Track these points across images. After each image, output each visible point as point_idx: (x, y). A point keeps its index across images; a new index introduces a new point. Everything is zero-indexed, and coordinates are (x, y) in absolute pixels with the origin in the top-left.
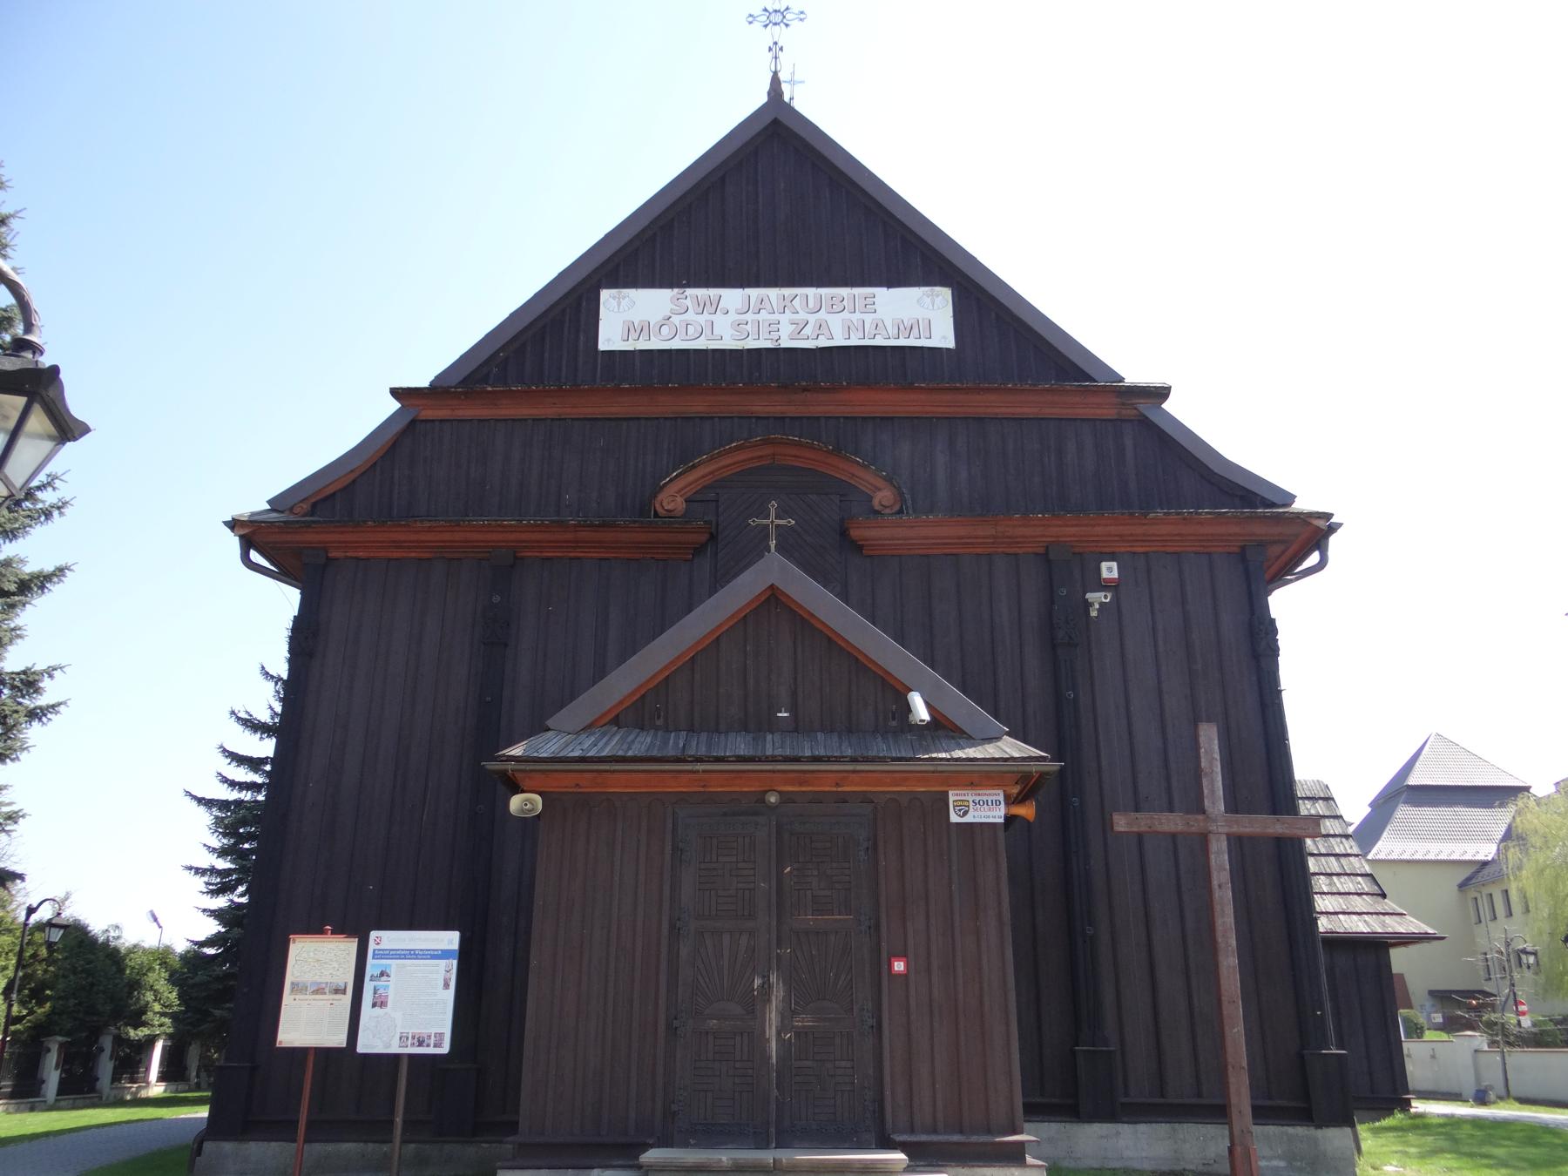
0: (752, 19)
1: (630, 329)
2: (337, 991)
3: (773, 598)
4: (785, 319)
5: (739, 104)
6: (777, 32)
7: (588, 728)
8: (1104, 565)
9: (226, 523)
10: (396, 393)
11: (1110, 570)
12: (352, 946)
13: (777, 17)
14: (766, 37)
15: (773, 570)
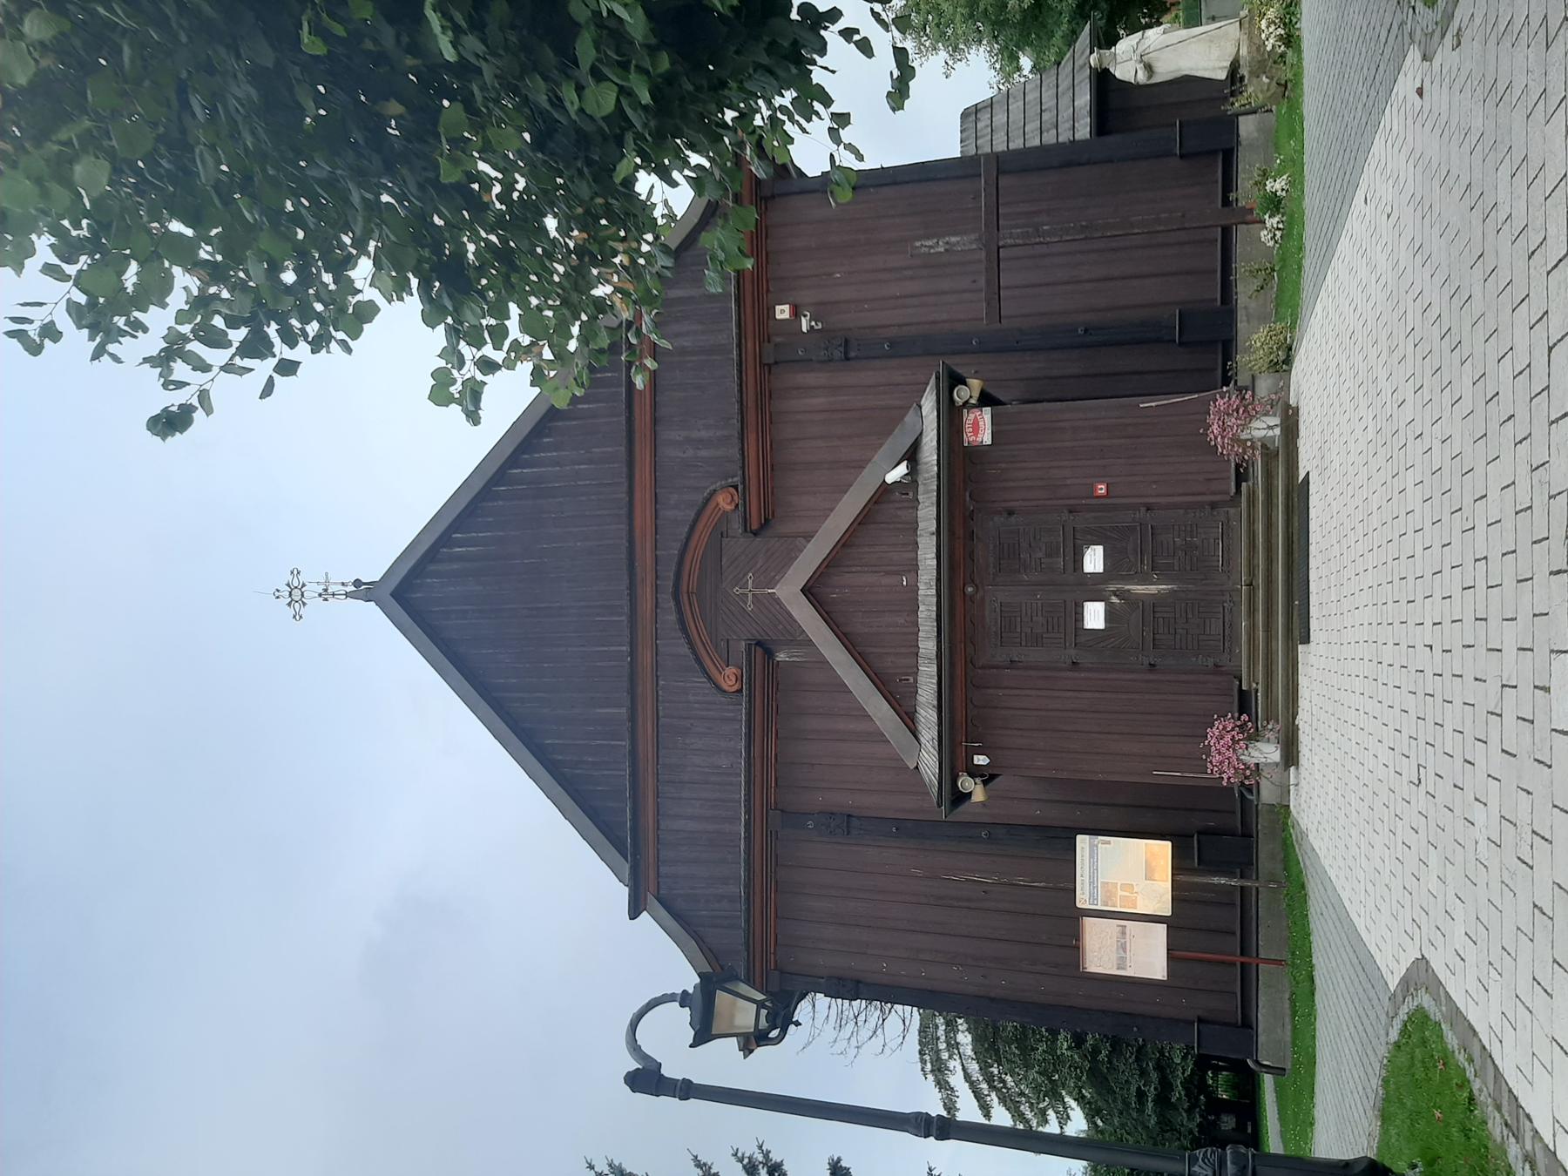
0: (297, 616)
2: (1124, 933)
5: (377, 630)
6: (312, 590)
7: (915, 734)
8: (779, 316)
10: (634, 914)
11: (782, 311)
12: (1088, 922)
13: (295, 595)
14: (314, 604)
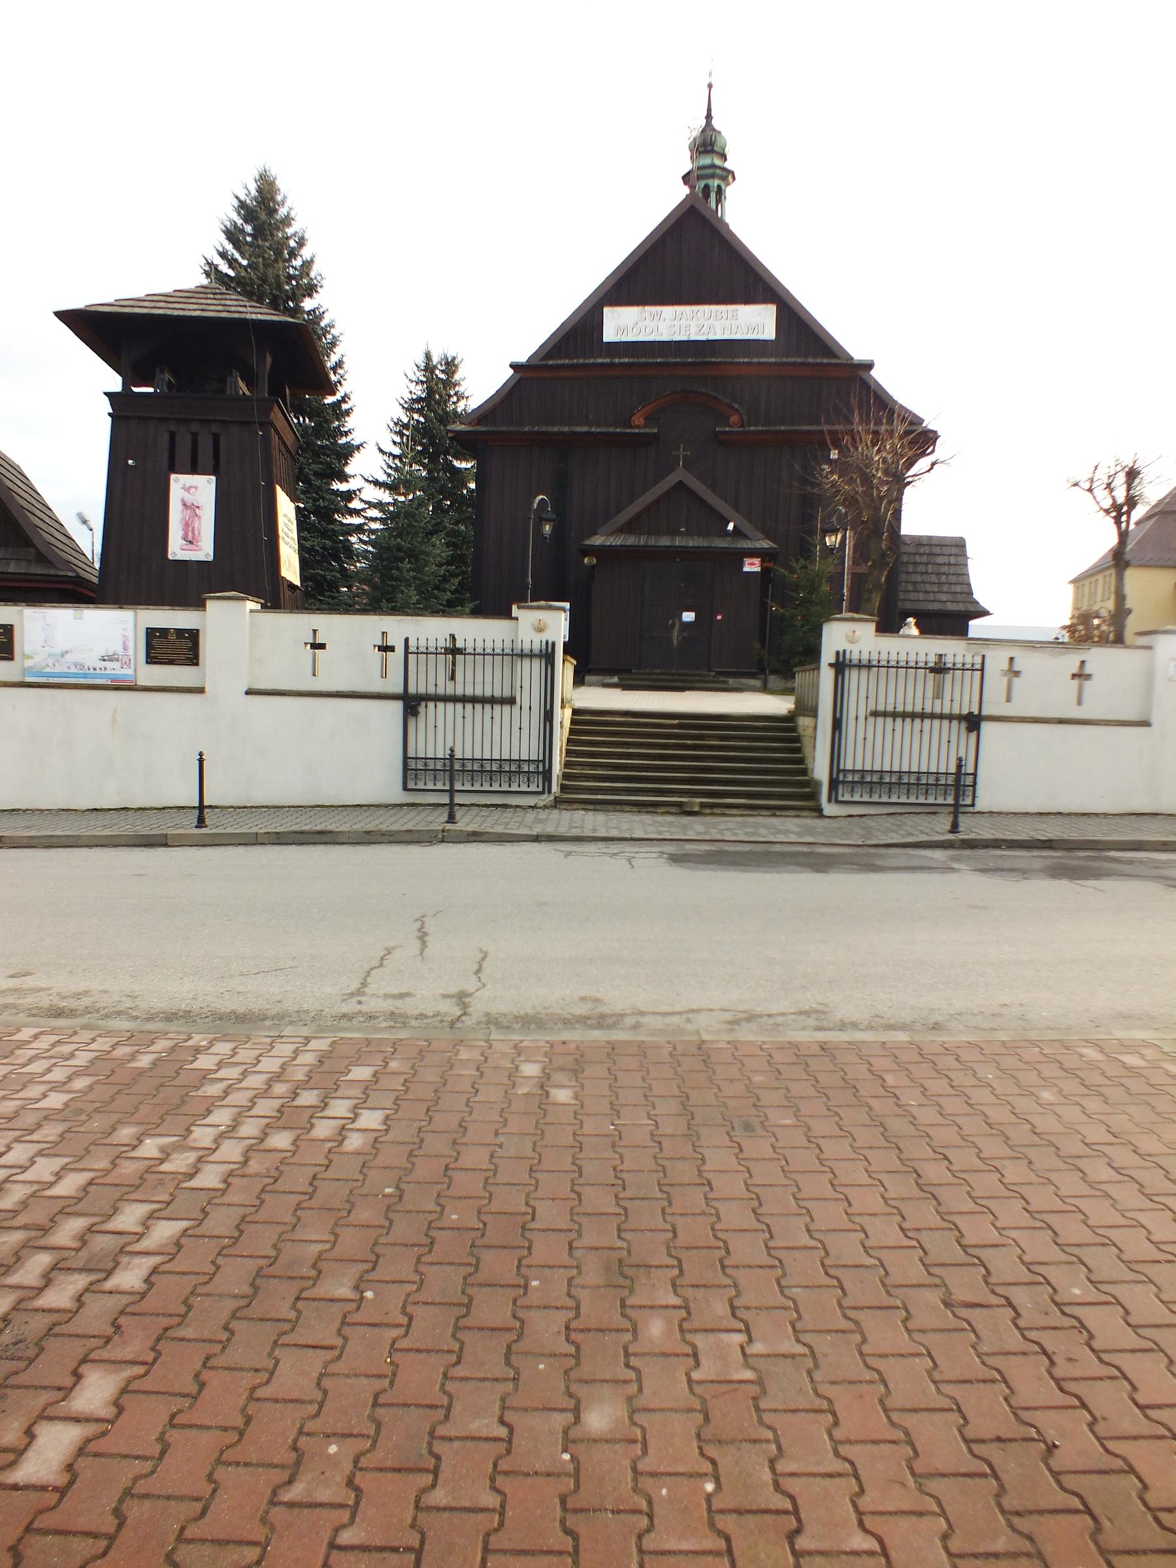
1: (618, 330)
3: (680, 483)
4: (693, 323)
7: (611, 534)
9: (267, 193)
15: (680, 474)
